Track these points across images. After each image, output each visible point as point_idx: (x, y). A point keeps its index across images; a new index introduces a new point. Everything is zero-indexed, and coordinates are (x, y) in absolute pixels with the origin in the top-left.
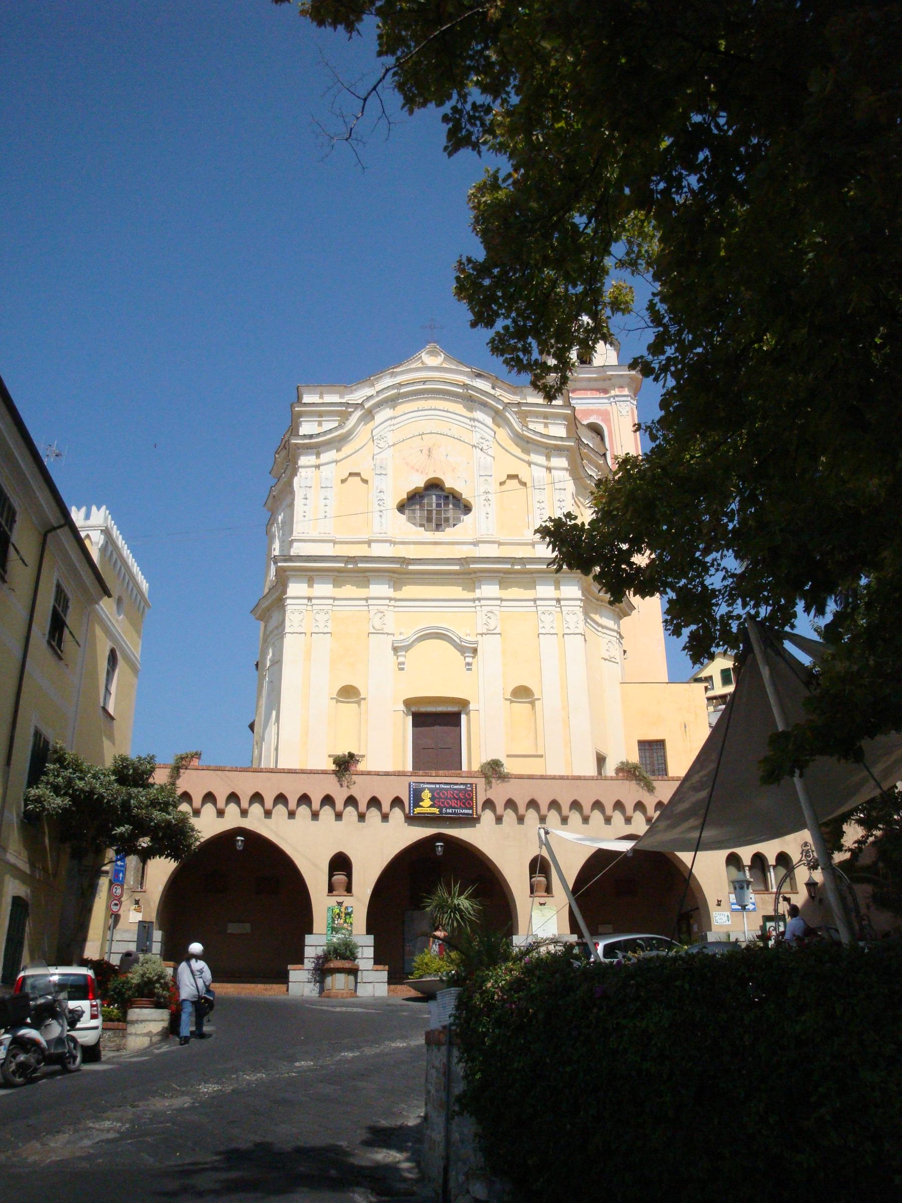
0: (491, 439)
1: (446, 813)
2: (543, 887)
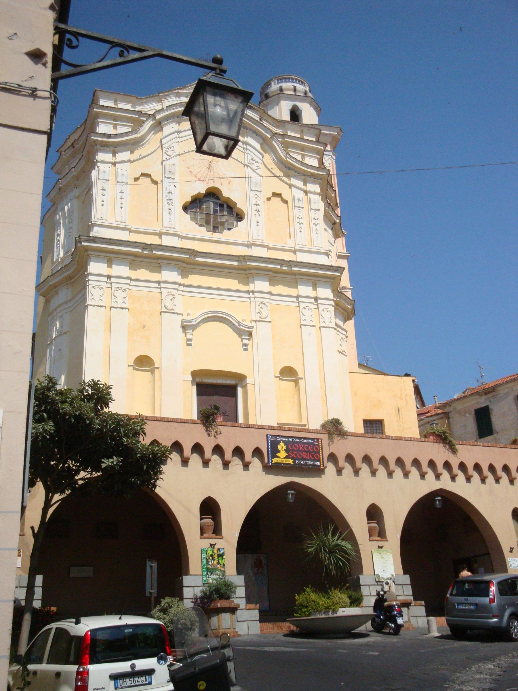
0: (261, 162)
1: (299, 464)
2: (211, 529)
